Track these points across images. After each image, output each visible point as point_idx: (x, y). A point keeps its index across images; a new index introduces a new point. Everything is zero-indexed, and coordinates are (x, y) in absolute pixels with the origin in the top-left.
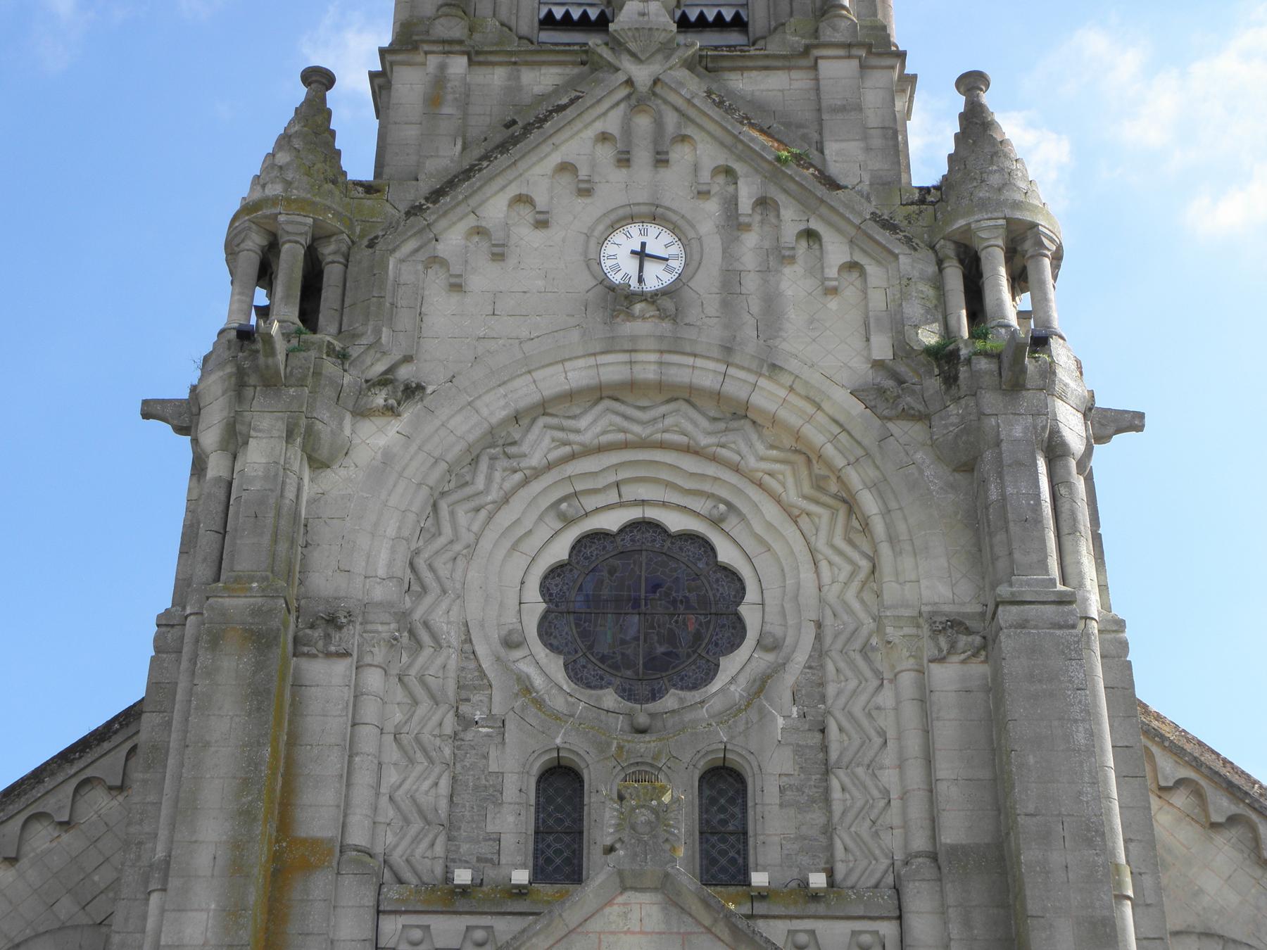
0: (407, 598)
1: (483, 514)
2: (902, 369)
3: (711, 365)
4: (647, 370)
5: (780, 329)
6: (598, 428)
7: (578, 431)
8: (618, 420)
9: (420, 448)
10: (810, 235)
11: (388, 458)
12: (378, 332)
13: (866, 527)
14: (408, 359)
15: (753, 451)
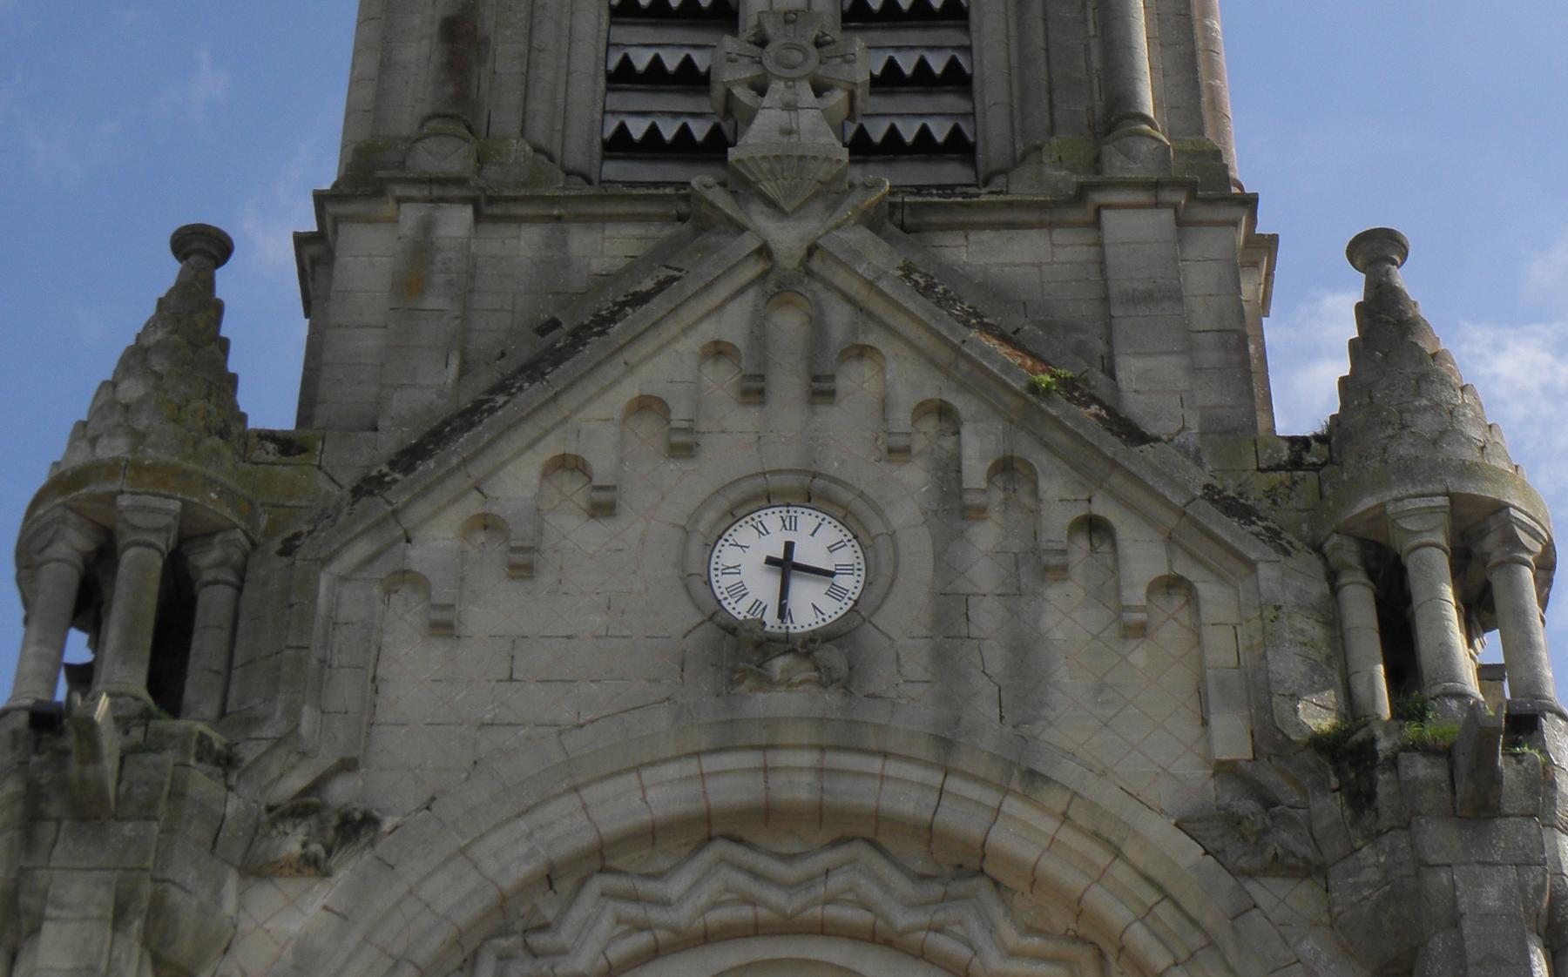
2: (1270, 777)
3: (915, 773)
4: (797, 788)
6: (703, 897)
7: (665, 903)
8: (741, 880)
9: (366, 939)
10: (1094, 527)
12: (293, 714)
14: (348, 765)
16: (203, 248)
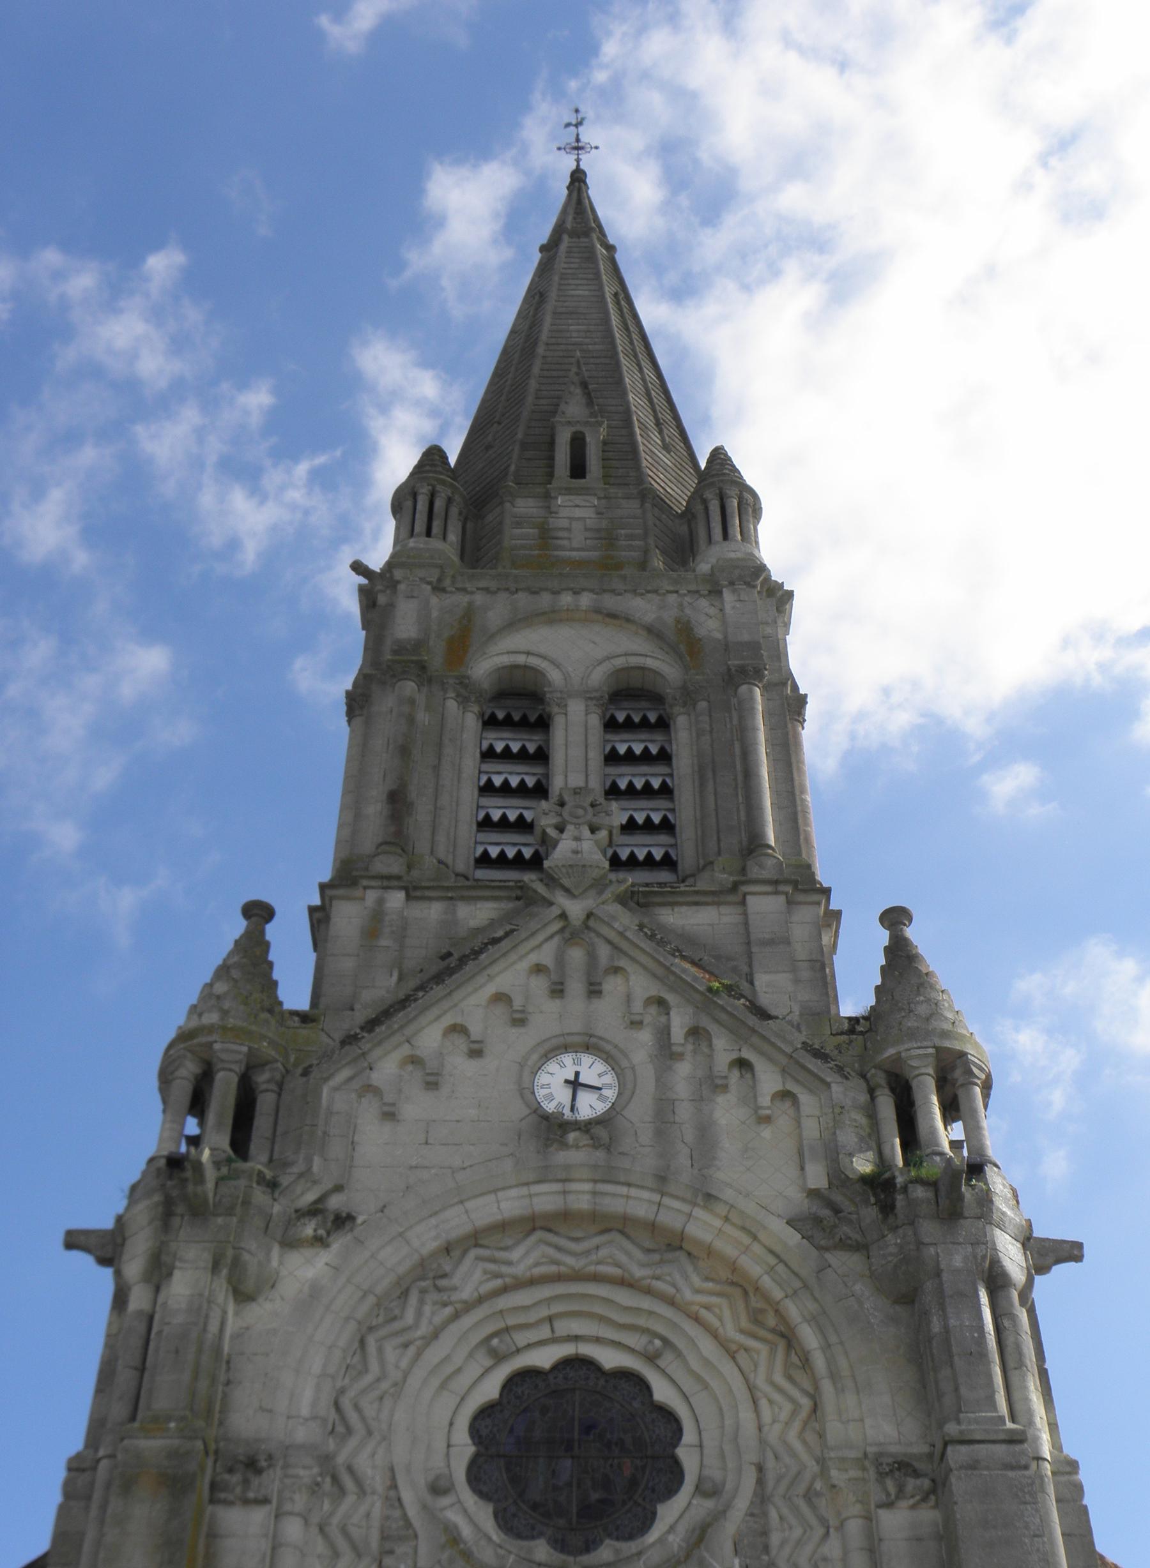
0: (331, 1440)
1: (412, 1350)
2: (837, 1198)
3: (646, 1195)
4: (582, 1203)
5: (714, 1158)
6: (530, 1261)
7: (509, 1263)
8: (551, 1252)
9: (348, 1281)
10: (743, 1064)
11: (315, 1291)
12: (309, 1161)
13: (806, 1362)
14: (338, 1189)
15: (689, 1284)
16: (259, 913)
